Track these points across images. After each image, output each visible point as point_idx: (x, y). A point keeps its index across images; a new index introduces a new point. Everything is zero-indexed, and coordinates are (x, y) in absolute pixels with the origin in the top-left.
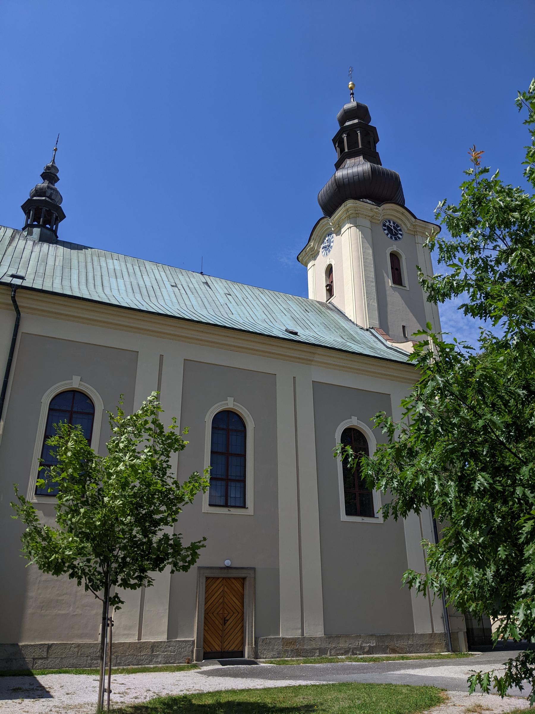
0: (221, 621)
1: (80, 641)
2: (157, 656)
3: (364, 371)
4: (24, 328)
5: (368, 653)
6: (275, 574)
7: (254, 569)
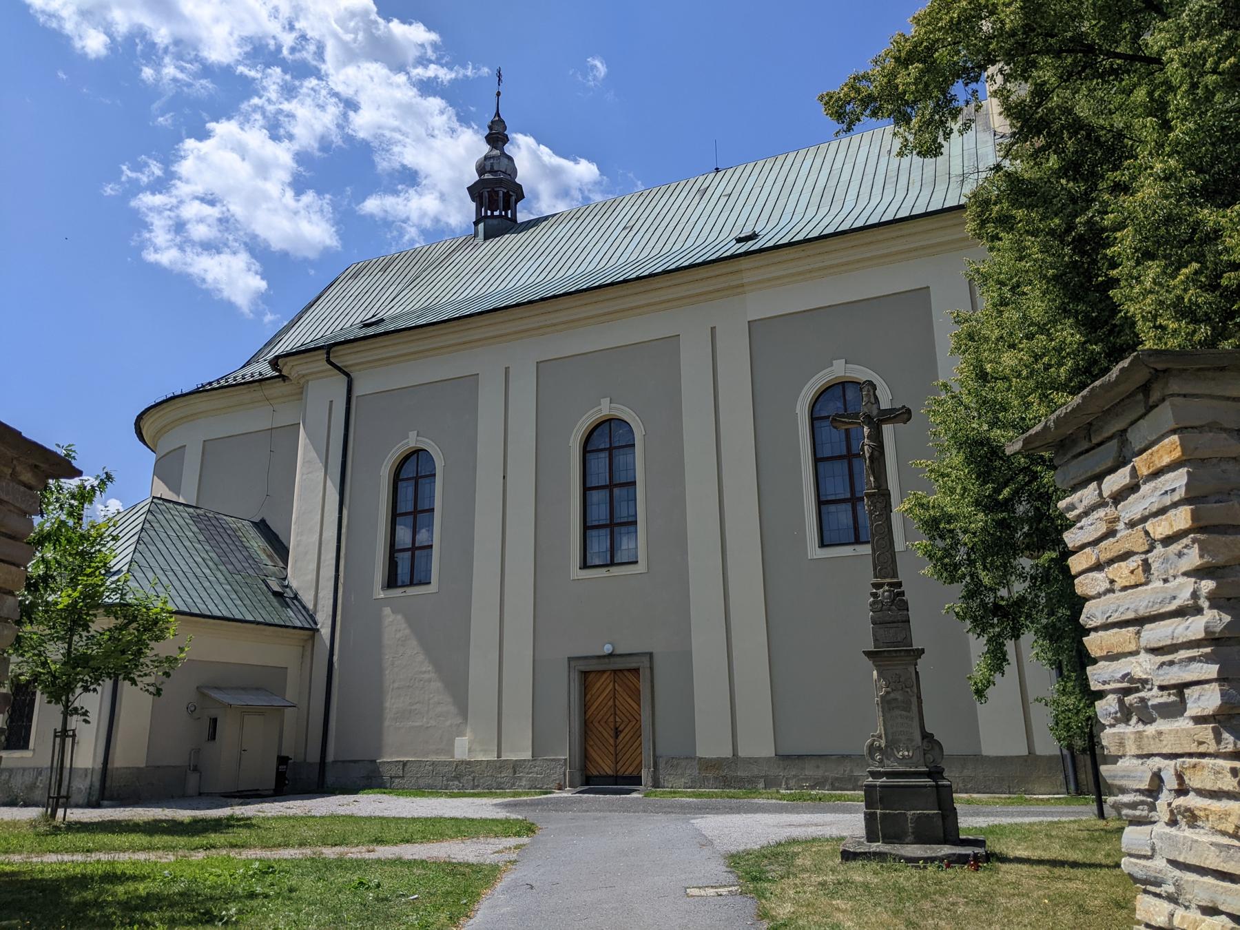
0: (612, 733)
1: (434, 758)
2: (520, 779)
3: (759, 282)
4: (358, 390)
6: (686, 657)
7: (651, 655)
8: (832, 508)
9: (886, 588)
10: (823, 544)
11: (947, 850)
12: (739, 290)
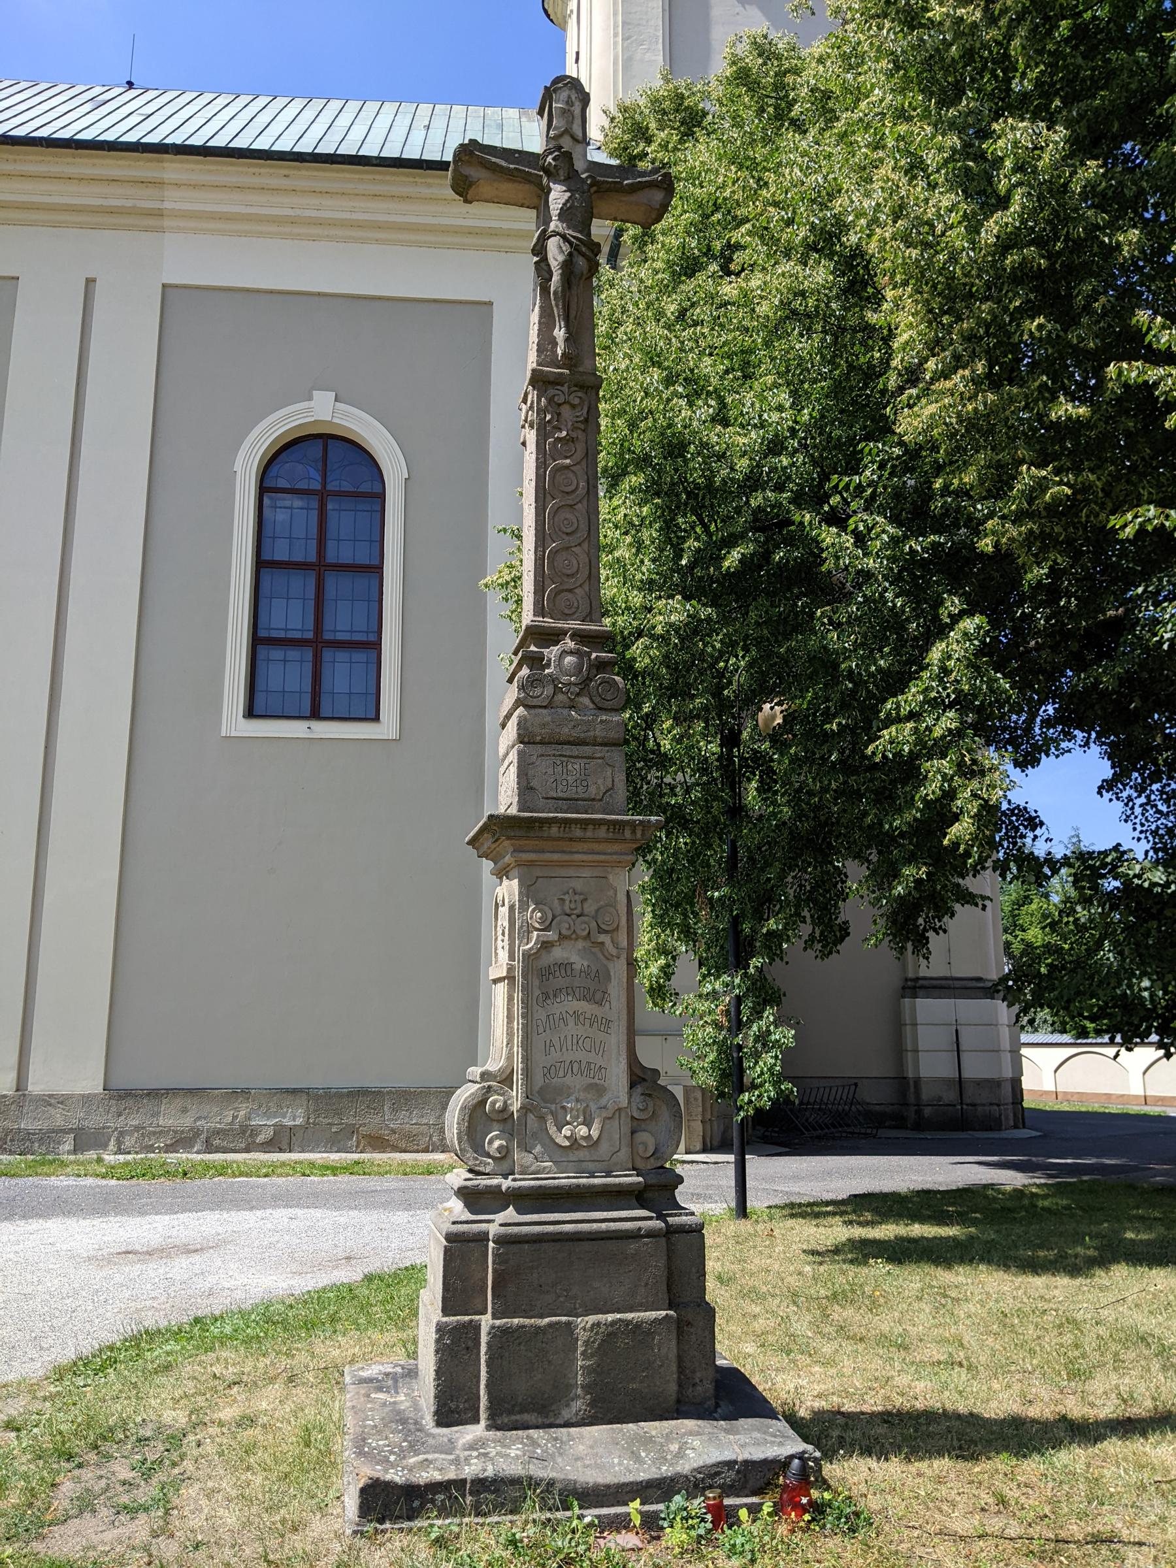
5: (272, 1145)
8: (277, 654)
9: (570, 644)
10: (251, 713)
11: (700, 1445)
12: (151, 222)
